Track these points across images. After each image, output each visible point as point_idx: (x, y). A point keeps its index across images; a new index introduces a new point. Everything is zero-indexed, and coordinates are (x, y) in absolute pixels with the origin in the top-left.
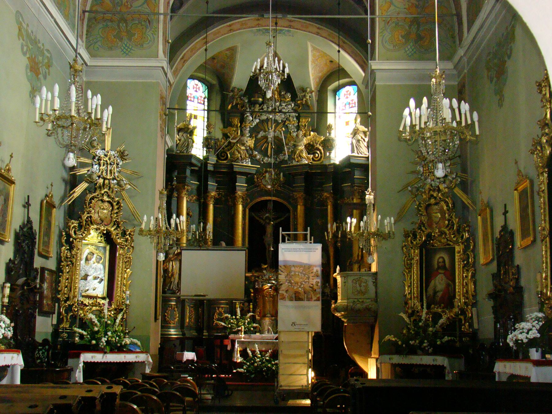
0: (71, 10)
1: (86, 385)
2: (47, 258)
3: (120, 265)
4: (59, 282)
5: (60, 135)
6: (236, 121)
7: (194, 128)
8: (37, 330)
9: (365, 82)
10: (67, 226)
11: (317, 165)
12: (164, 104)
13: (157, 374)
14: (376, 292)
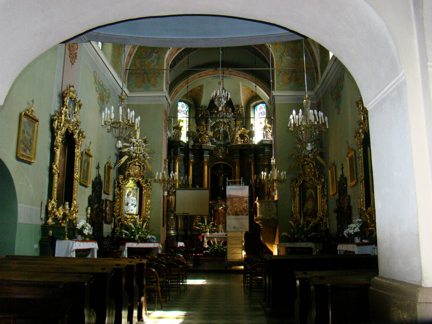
0: (120, 70)
1: (129, 259)
2: (108, 194)
3: (145, 197)
4: (114, 207)
5: (114, 132)
6: (203, 123)
7: (182, 127)
8: (104, 231)
9: (270, 101)
10: (118, 178)
11: (245, 145)
12: (166, 115)
13: (164, 254)
14: (277, 210)
